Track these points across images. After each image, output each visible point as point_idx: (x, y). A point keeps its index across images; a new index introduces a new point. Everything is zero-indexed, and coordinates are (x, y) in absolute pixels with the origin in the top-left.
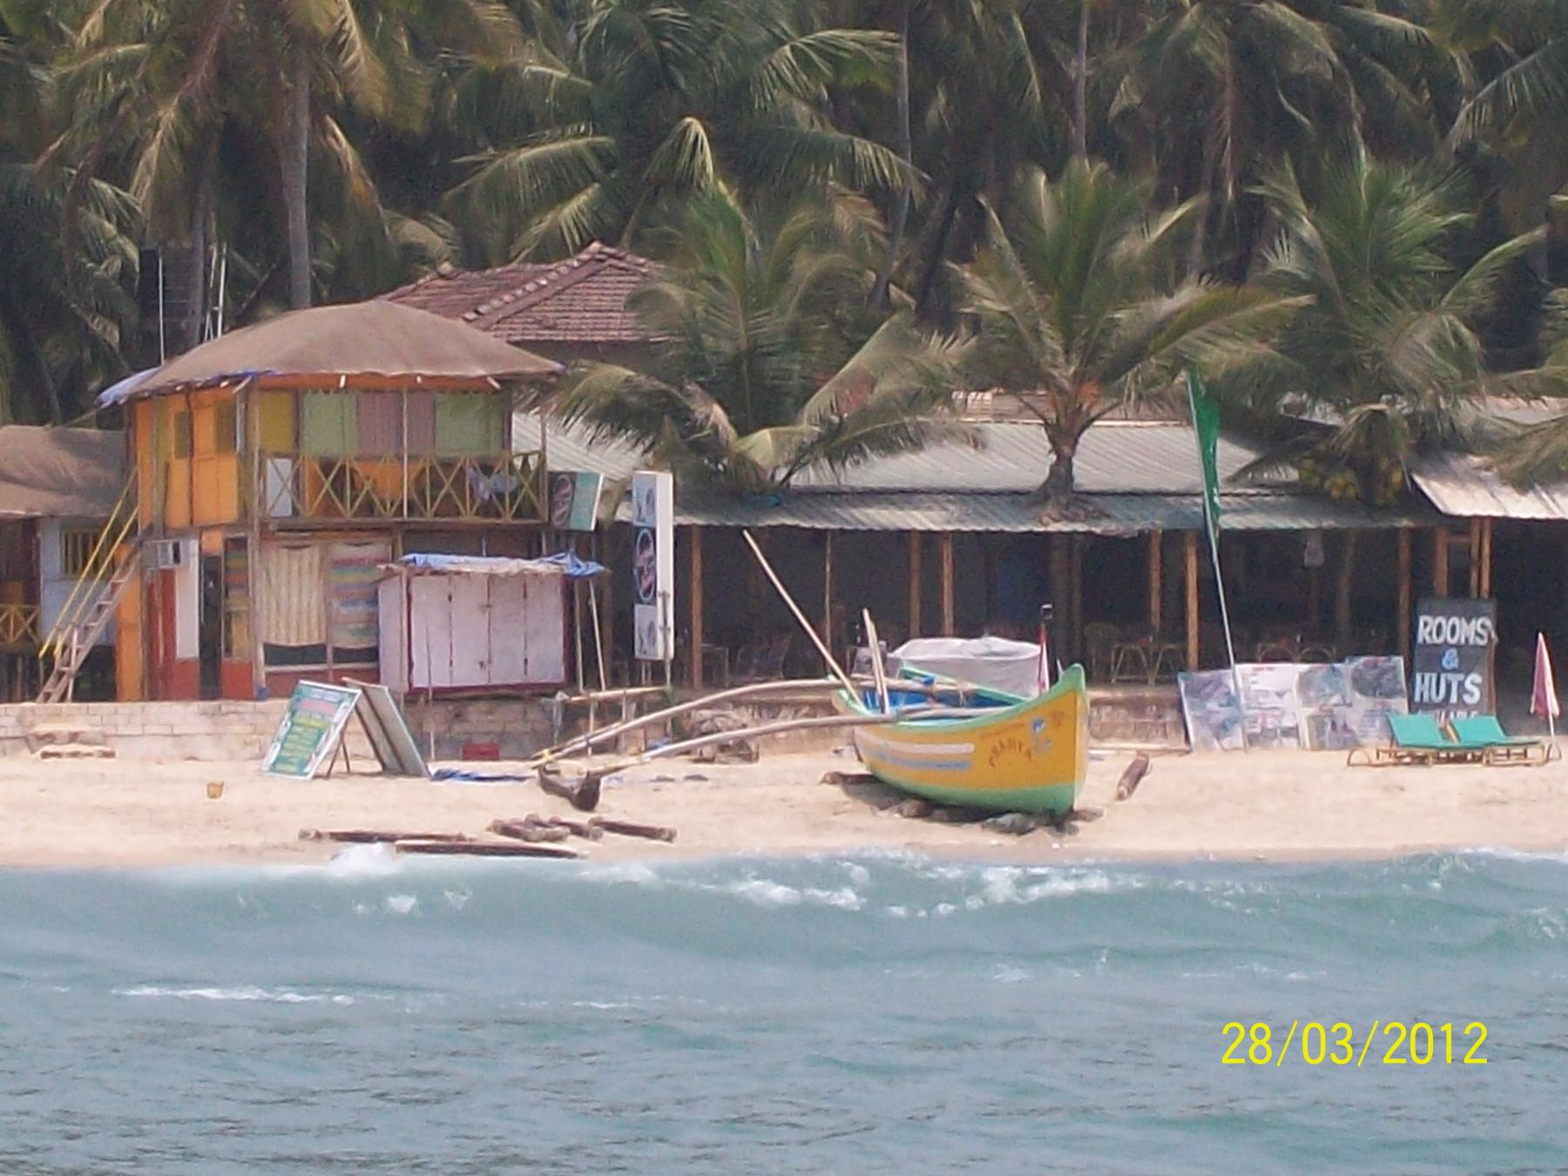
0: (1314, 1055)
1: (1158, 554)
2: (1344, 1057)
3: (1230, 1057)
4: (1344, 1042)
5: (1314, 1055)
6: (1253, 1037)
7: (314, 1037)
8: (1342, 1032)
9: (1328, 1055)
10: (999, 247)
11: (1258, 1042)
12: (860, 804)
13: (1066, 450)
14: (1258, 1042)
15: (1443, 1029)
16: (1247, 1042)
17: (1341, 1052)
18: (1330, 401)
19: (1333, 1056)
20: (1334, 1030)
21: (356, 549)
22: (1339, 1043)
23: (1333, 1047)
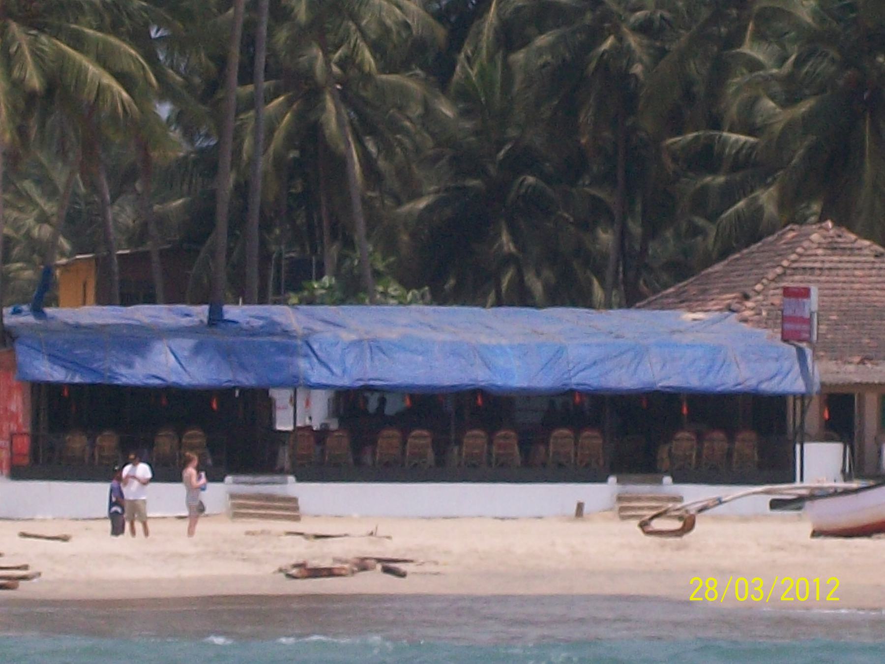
0: (741, 596)
1: (256, 486)
2: (758, 597)
3: (695, 597)
4: (759, 589)
5: (741, 596)
6: (707, 585)
7: (828, 278)
8: (757, 584)
9: (749, 596)
10: (134, 222)
11: (710, 589)
12: (558, 384)
13: (279, 329)
14: (713, 589)
15: (814, 581)
16: (704, 588)
17: (757, 594)
18: (361, 292)
19: (753, 596)
20: (753, 581)
21: (263, 67)
22: (756, 589)
23: (752, 591)
